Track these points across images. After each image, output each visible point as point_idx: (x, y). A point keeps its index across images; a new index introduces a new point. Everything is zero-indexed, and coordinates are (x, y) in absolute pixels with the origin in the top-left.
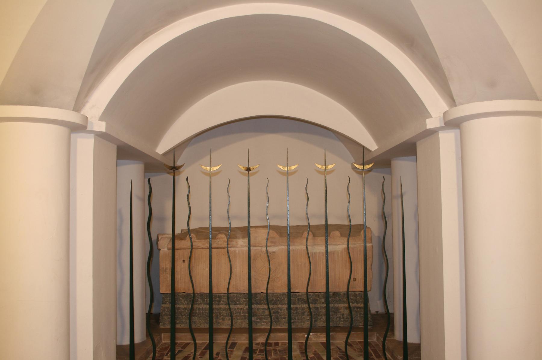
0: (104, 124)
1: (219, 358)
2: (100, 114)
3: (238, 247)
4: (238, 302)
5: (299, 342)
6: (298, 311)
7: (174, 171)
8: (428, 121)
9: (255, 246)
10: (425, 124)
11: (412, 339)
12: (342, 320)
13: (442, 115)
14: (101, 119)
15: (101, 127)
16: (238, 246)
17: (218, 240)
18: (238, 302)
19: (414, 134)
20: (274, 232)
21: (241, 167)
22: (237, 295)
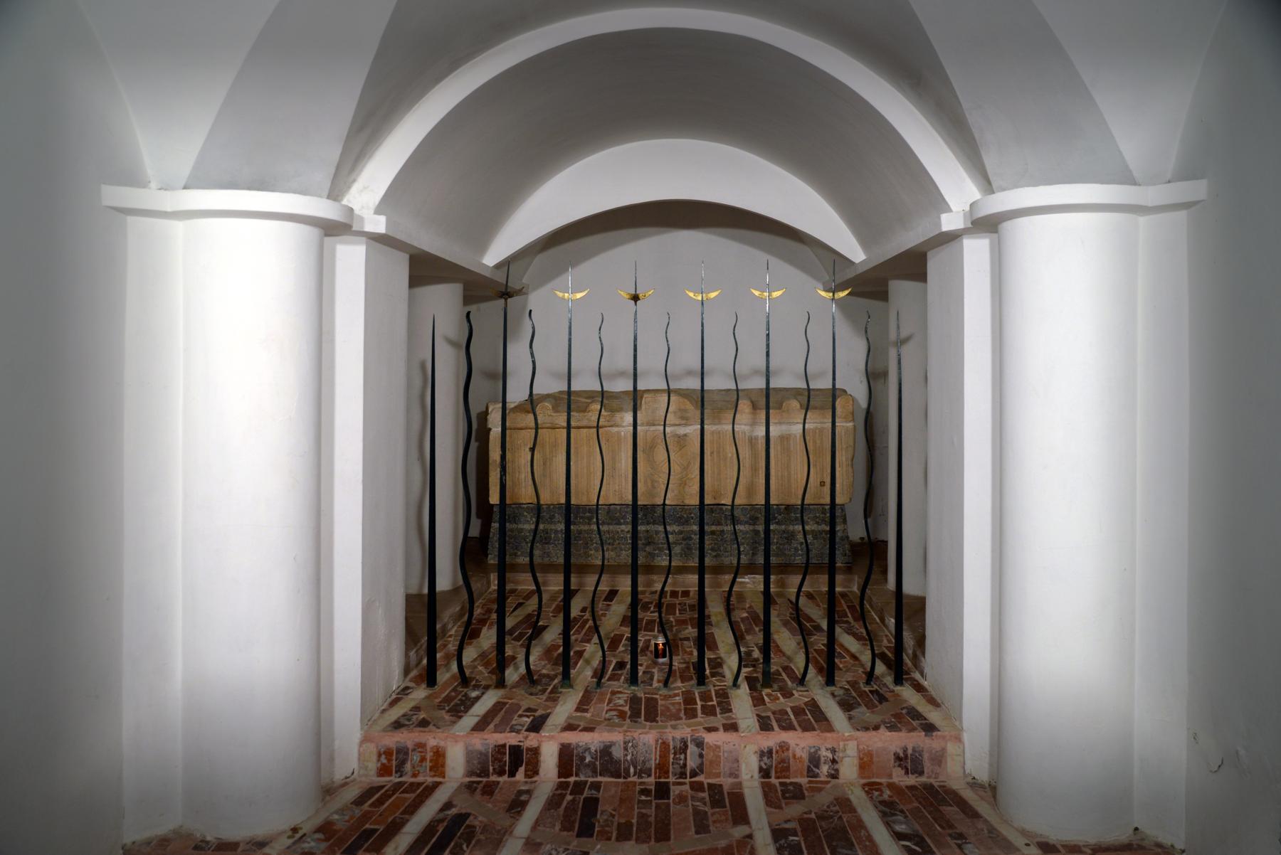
0: (382, 219)
1: (585, 618)
2: (377, 203)
3: (623, 427)
4: (622, 521)
5: (724, 589)
6: (725, 536)
7: (506, 300)
8: (944, 217)
9: (654, 425)
10: (939, 224)
11: (909, 588)
12: (800, 552)
13: (967, 208)
14: (378, 211)
15: (378, 225)
16: (624, 424)
17: (590, 414)
18: (622, 521)
19: (922, 240)
20: (686, 400)
21: (622, 293)
22: (621, 508)
